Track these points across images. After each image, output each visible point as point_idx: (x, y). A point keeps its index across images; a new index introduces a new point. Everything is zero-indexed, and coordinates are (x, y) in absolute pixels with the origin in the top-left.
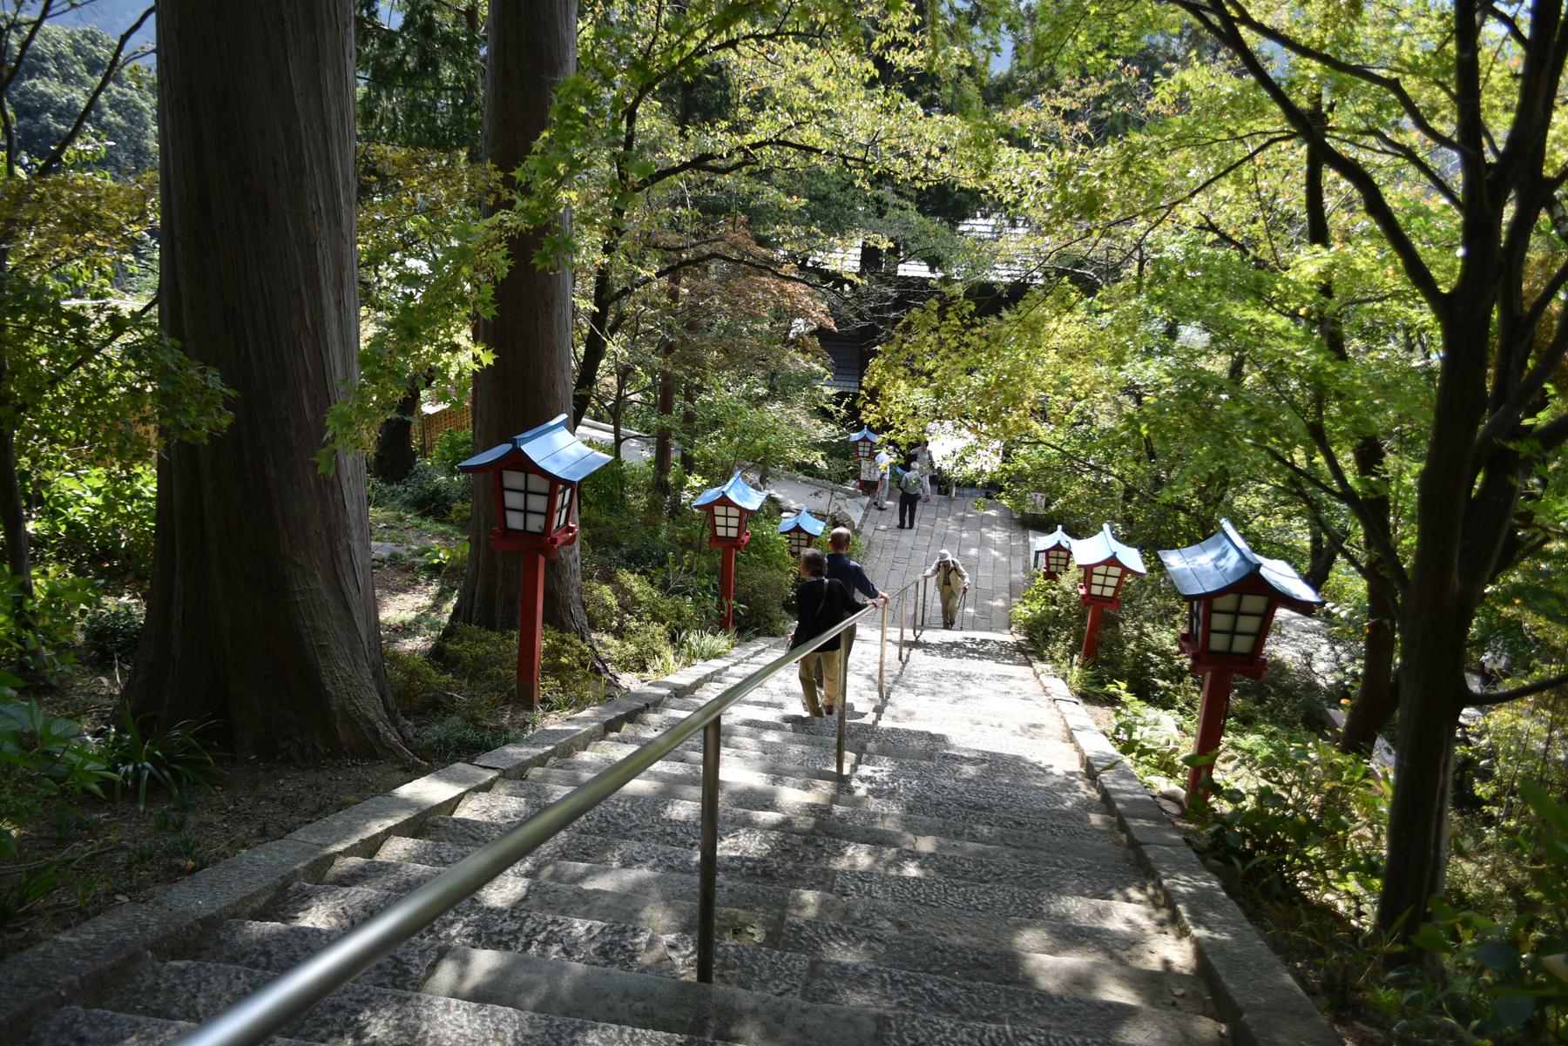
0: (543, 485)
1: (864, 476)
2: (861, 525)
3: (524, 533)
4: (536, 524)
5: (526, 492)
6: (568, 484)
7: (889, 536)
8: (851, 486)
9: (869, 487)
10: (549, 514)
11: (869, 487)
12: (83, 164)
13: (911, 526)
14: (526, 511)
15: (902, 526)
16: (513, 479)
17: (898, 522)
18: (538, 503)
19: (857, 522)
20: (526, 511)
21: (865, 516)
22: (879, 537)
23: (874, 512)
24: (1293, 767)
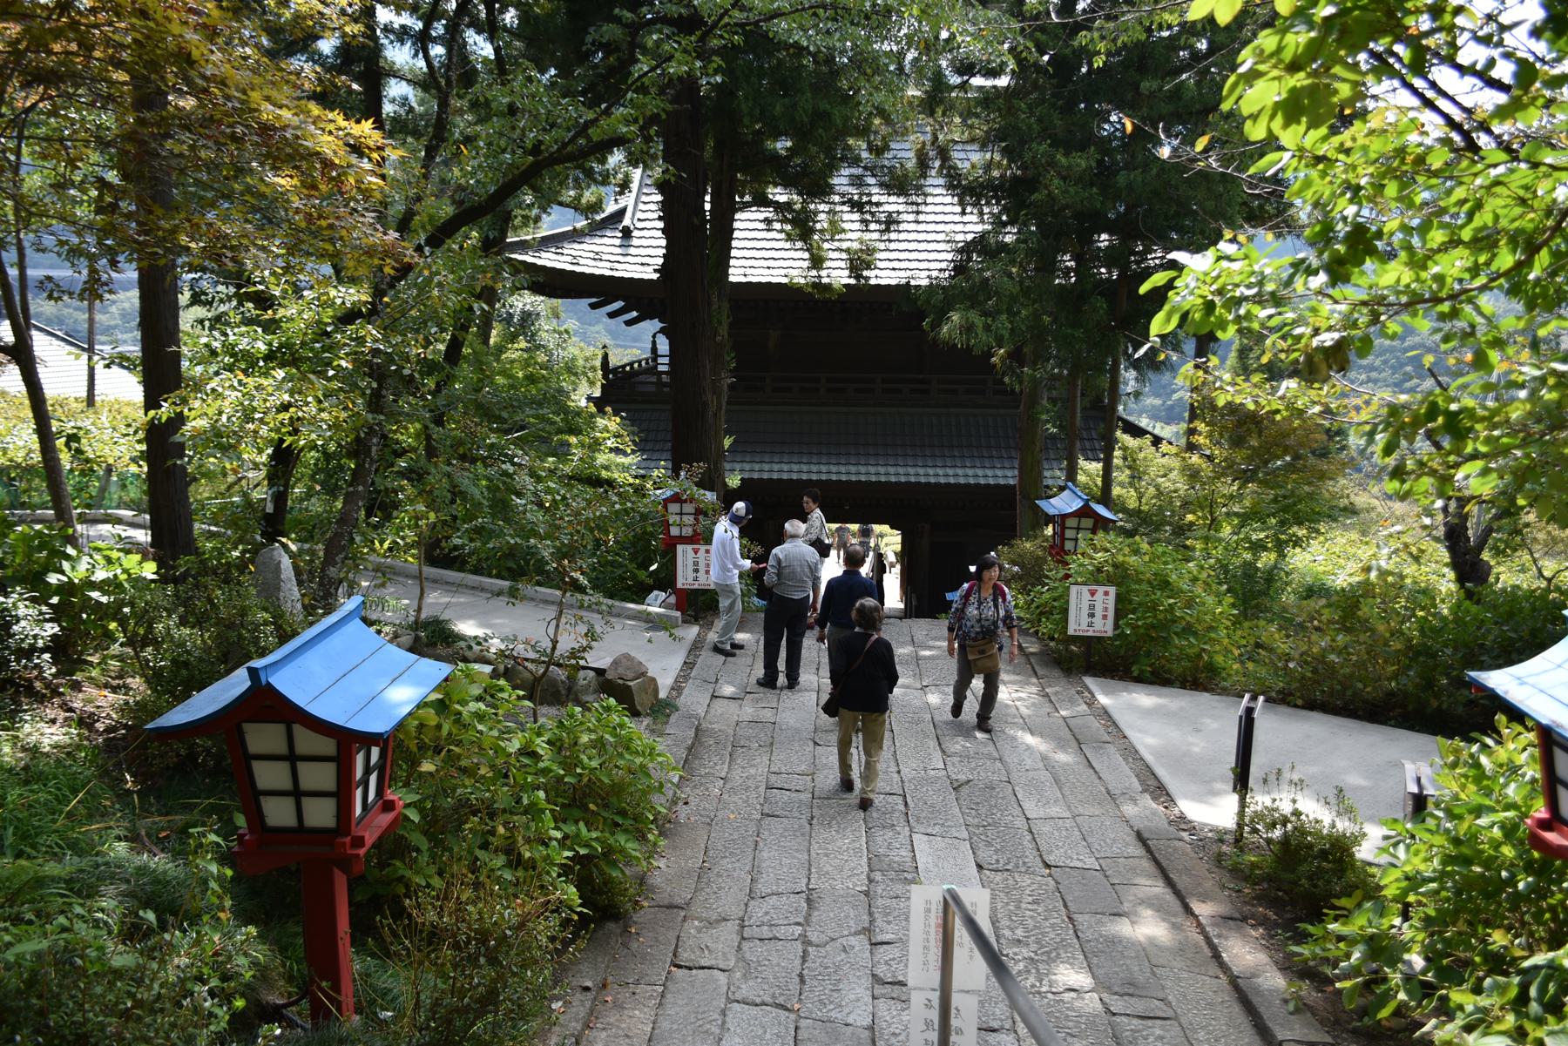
0: (328, 746)
1: (684, 579)
2: (677, 688)
3: (301, 832)
4: (320, 814)
5: (292, 758)
6: (368, 739)
7: (748, 711)
8: (655, 605)
9: (699, 605)
10: (342, 795)
11: (699, 605)
12: (284, 546)
13: (793, 681)
14: (297, 793)
15: (769, 681)
16: (262, 737)
17: (760, 672)
18: (320, 776)
19: (665, 683)
20: (297, 793)
21: (688, 665)
22: (725, 716)
23: (708, 660)
24: (1114, 529)
